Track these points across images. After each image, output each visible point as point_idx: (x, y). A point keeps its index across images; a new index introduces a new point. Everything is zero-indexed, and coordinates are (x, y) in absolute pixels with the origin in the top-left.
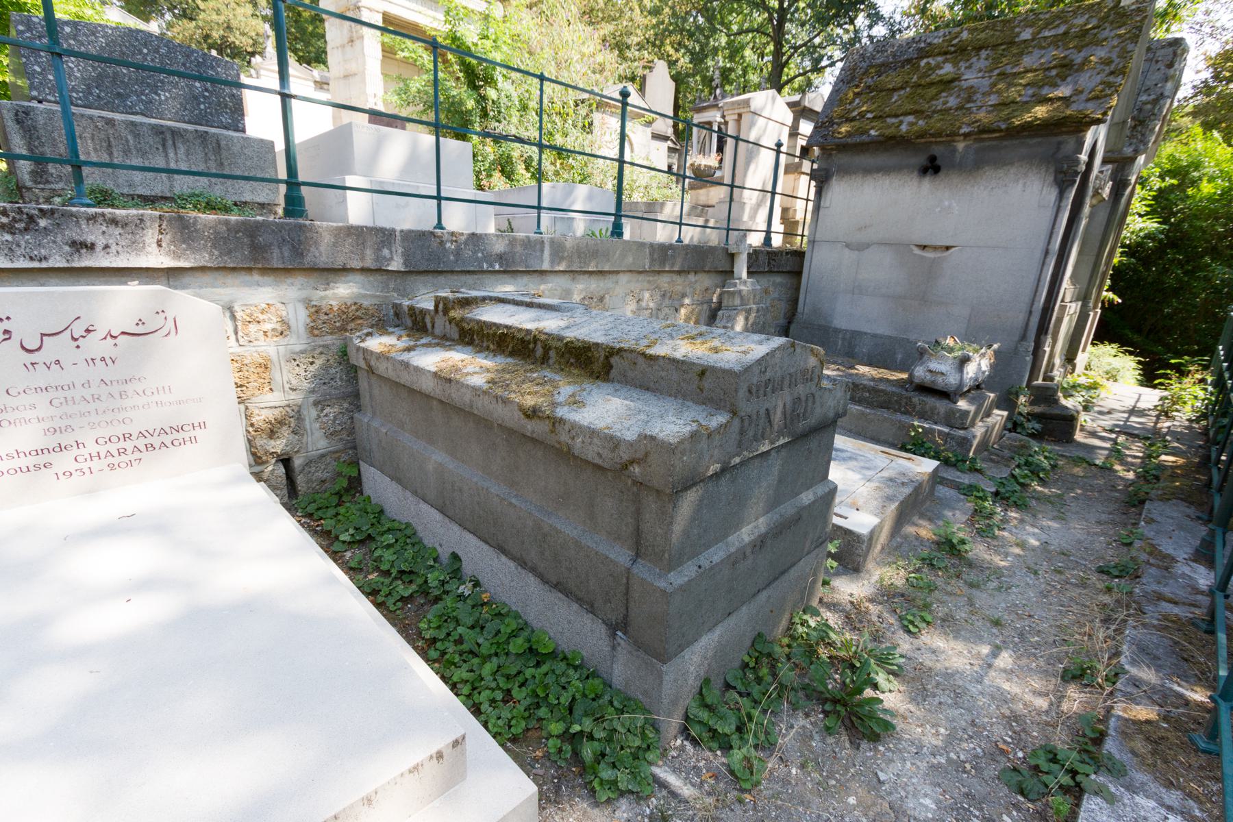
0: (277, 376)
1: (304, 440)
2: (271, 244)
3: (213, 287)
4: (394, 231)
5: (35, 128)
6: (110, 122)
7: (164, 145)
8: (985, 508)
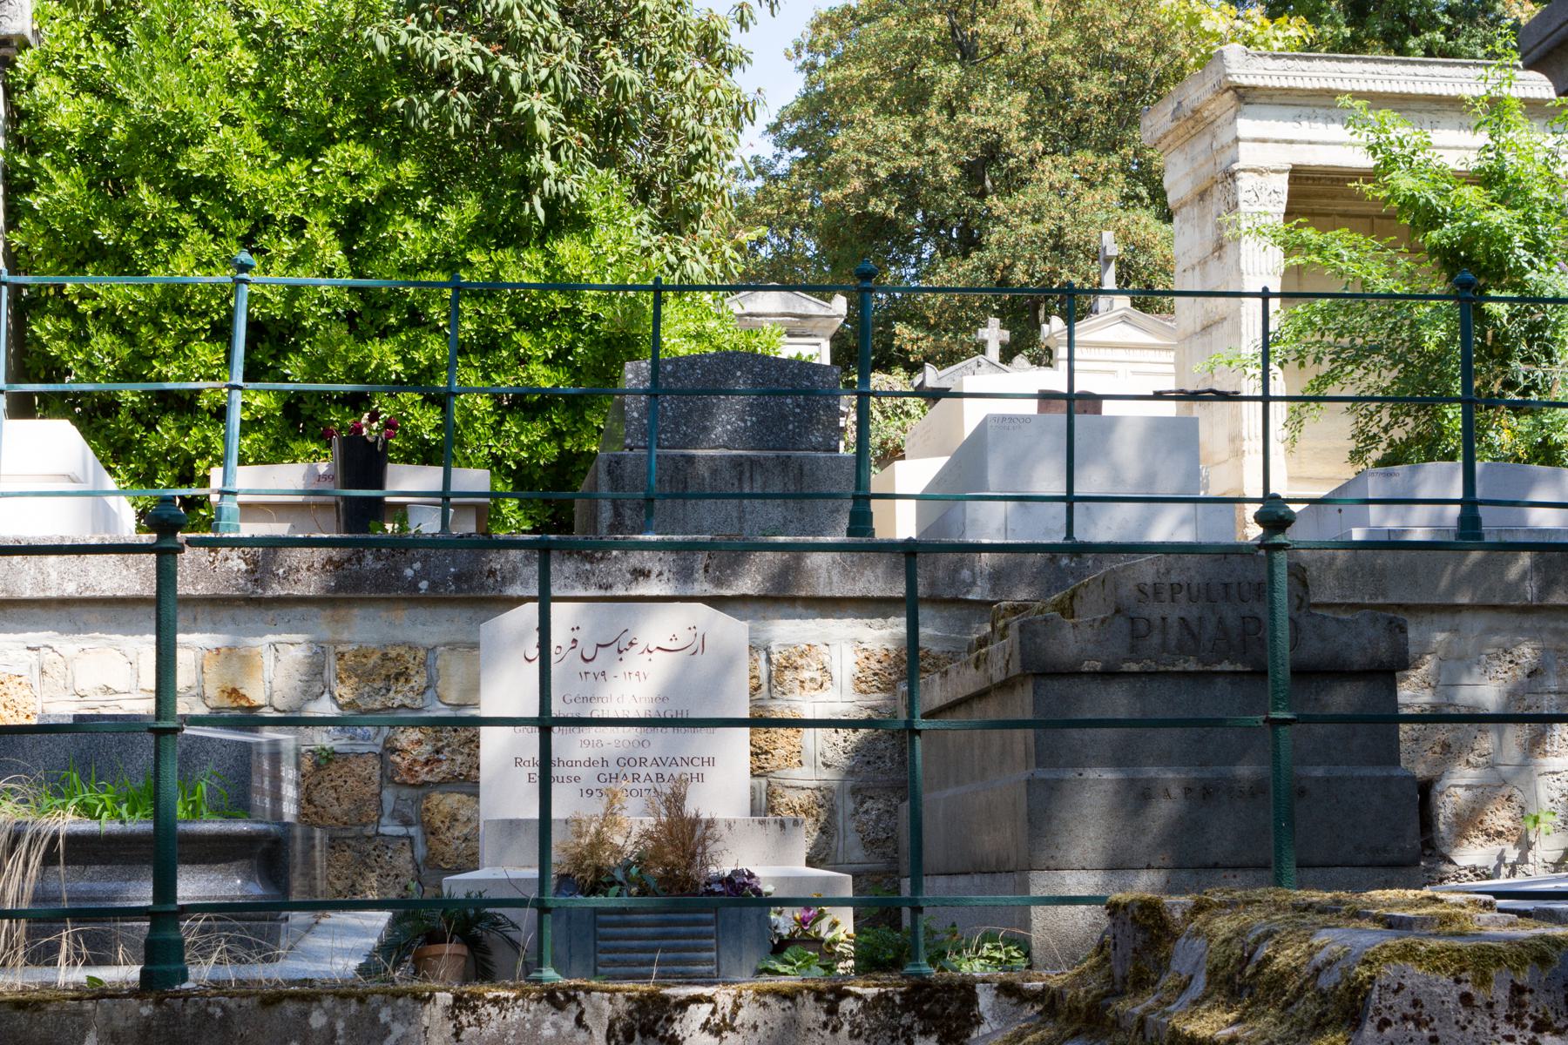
1: (834, 845)
7: (740, 480)
8: (407, 295)
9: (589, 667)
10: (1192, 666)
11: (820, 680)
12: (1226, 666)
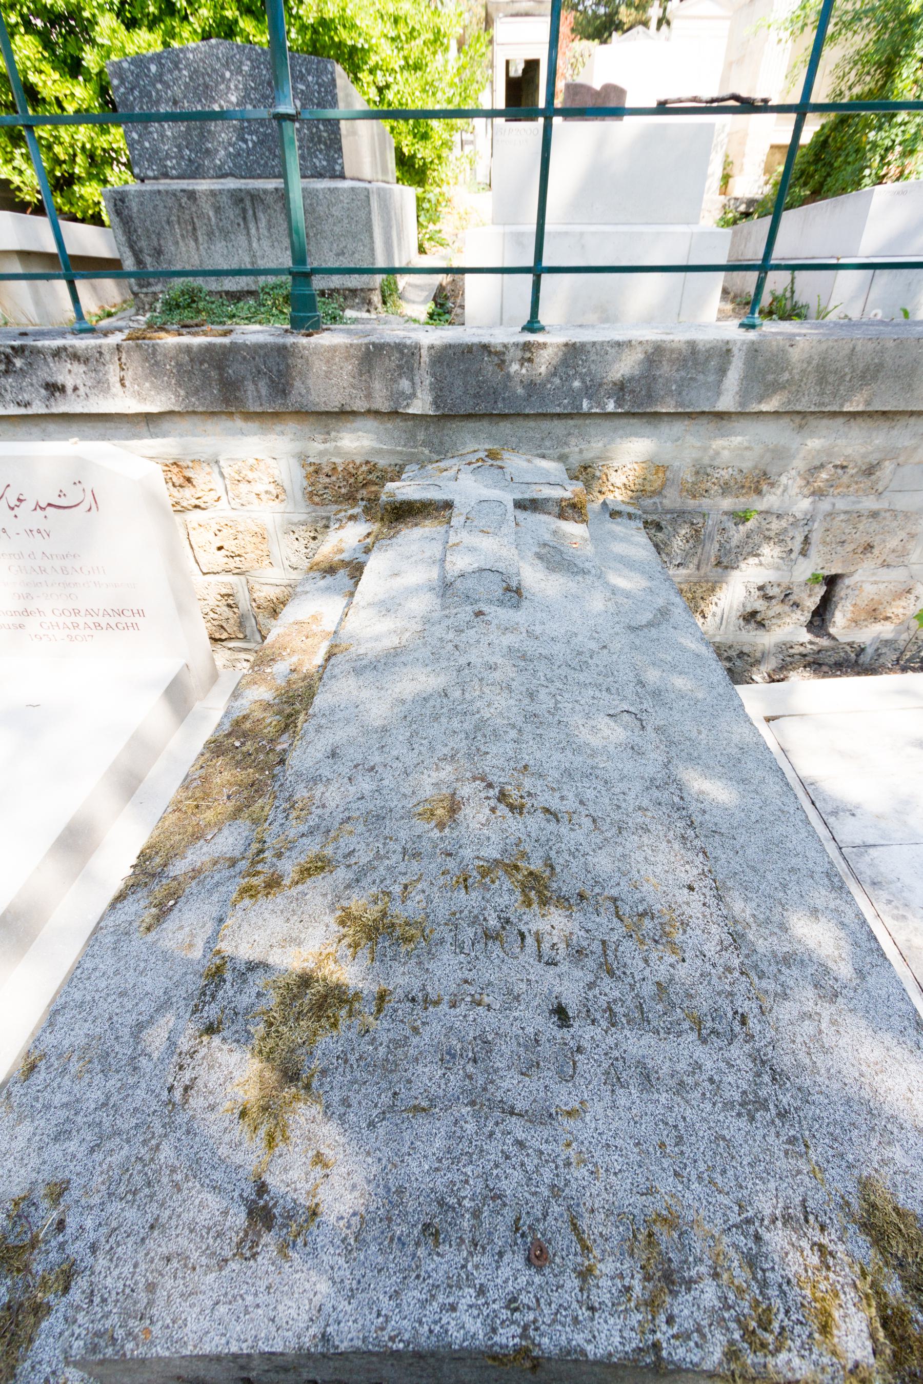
0: (275, 550)
2: (244, 378)
3: (195, 436)
4: (418, 347)
5: (131, 217)
6: (192, 195)
7: (244, 219)
11: (274, 492)
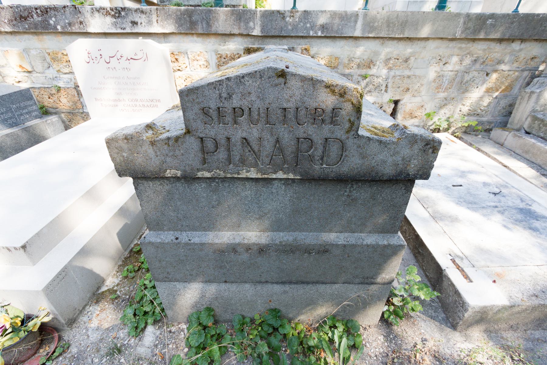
9: (109, 65)
10: (253, 174)
12: (280, 175)
